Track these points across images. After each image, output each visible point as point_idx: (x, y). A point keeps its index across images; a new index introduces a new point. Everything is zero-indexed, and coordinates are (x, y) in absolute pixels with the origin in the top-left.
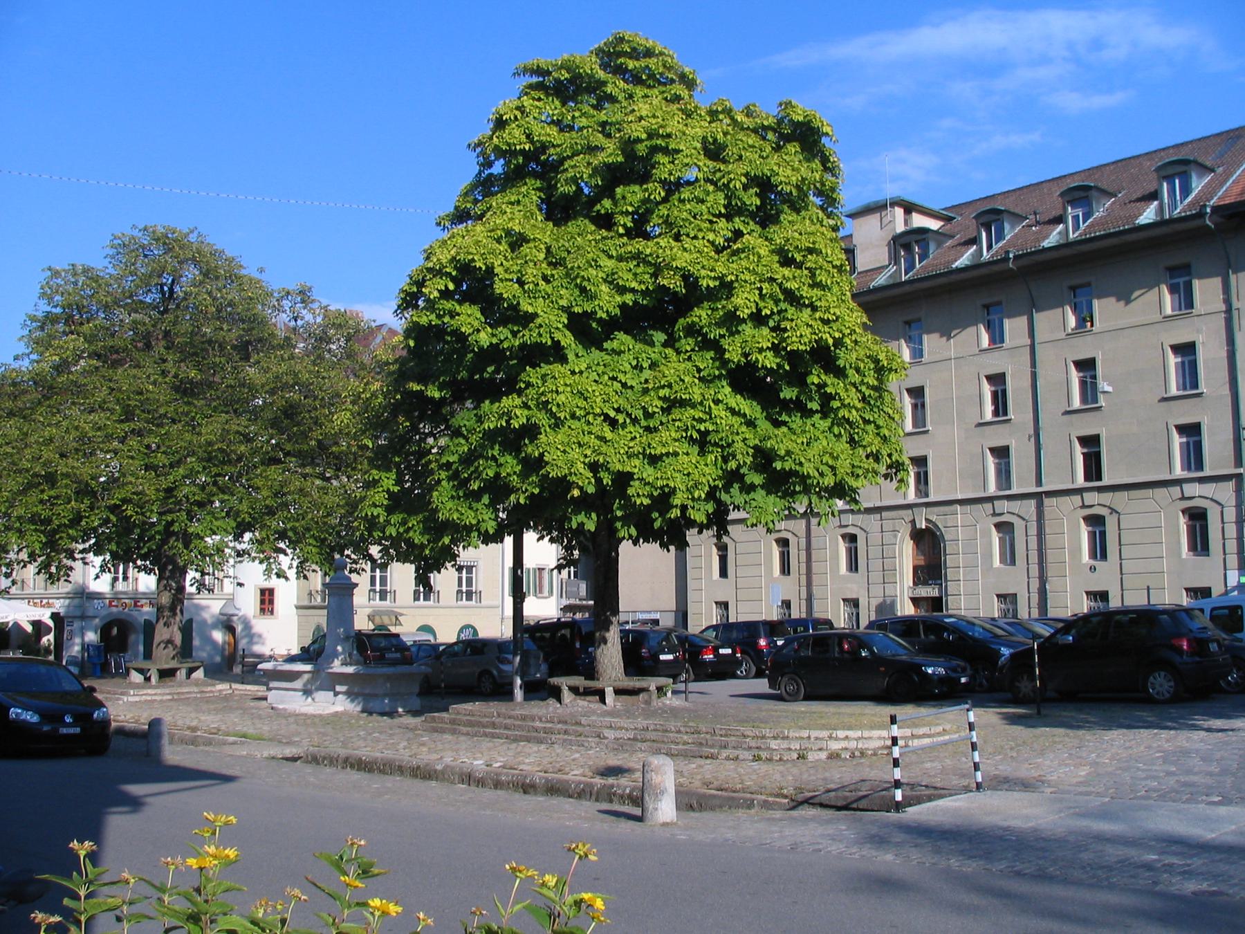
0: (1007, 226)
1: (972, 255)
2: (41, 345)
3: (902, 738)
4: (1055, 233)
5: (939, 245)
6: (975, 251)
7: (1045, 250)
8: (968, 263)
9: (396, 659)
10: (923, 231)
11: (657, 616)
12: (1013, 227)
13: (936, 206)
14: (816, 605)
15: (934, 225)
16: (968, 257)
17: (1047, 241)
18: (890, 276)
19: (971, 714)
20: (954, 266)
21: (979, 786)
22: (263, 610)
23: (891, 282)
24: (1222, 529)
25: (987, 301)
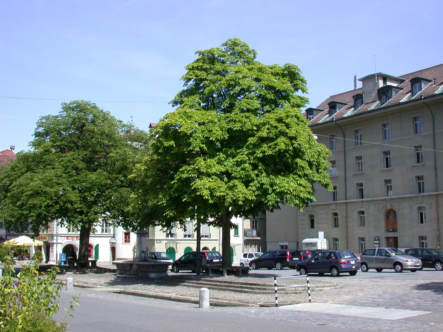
0: (423, 85)
1: (408, 97)
2: (36, 144)
3: (311, 287)
4: (441, 88)
5: (397, 92)
6: (410, 95)
7: (344, 118)
8: (406, 100)
9: (317, 275)
10: (391, 87)
11: (286, 244)
12: (425, 85)
13: (396, 75)
14: (204, 238)
15: (395, 85)
16: (406, 98)
17: (321, 121)
18: (377, 106)
19: (308, 278)
20: (401, 102)
21: (310, 301)
22: (126, 241)
23: (377, 108)
24: (429, 214)
25: (415, 116)
